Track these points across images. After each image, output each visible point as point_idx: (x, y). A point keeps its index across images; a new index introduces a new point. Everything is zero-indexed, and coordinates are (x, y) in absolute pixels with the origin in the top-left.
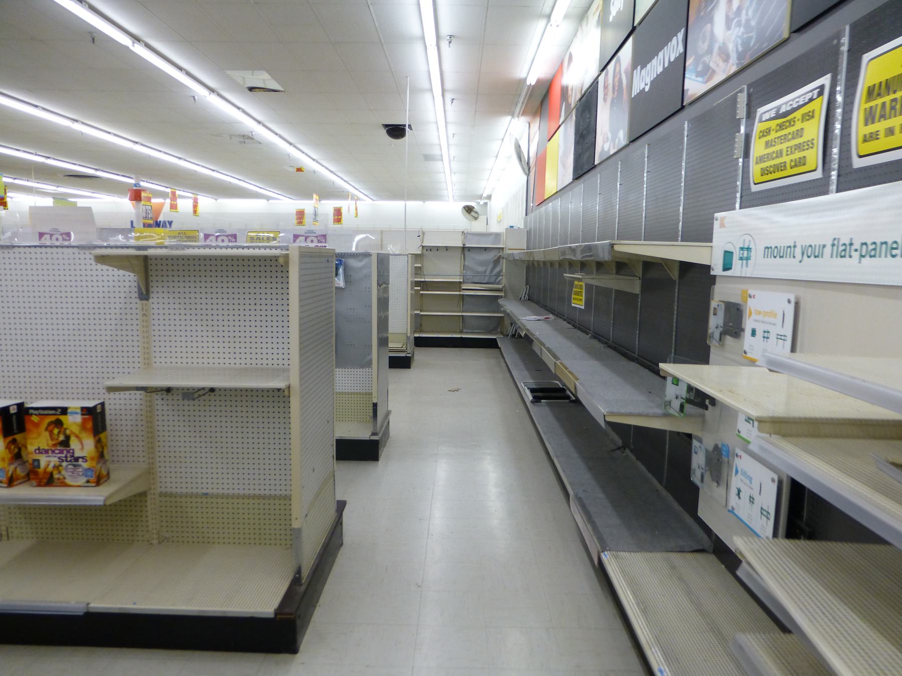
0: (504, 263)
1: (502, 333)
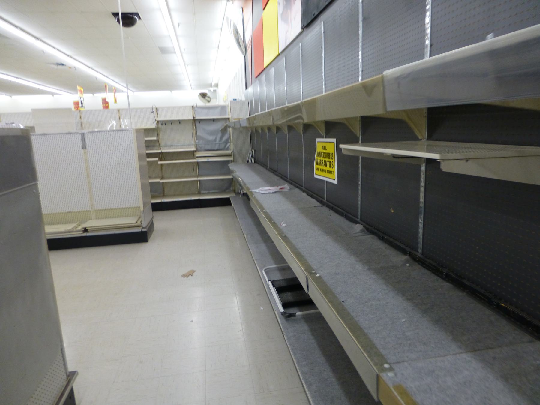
0: (230, 131)
1: (234, 191)
